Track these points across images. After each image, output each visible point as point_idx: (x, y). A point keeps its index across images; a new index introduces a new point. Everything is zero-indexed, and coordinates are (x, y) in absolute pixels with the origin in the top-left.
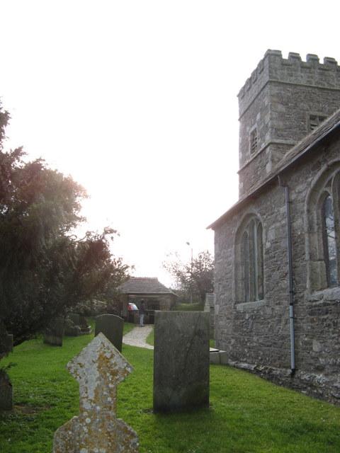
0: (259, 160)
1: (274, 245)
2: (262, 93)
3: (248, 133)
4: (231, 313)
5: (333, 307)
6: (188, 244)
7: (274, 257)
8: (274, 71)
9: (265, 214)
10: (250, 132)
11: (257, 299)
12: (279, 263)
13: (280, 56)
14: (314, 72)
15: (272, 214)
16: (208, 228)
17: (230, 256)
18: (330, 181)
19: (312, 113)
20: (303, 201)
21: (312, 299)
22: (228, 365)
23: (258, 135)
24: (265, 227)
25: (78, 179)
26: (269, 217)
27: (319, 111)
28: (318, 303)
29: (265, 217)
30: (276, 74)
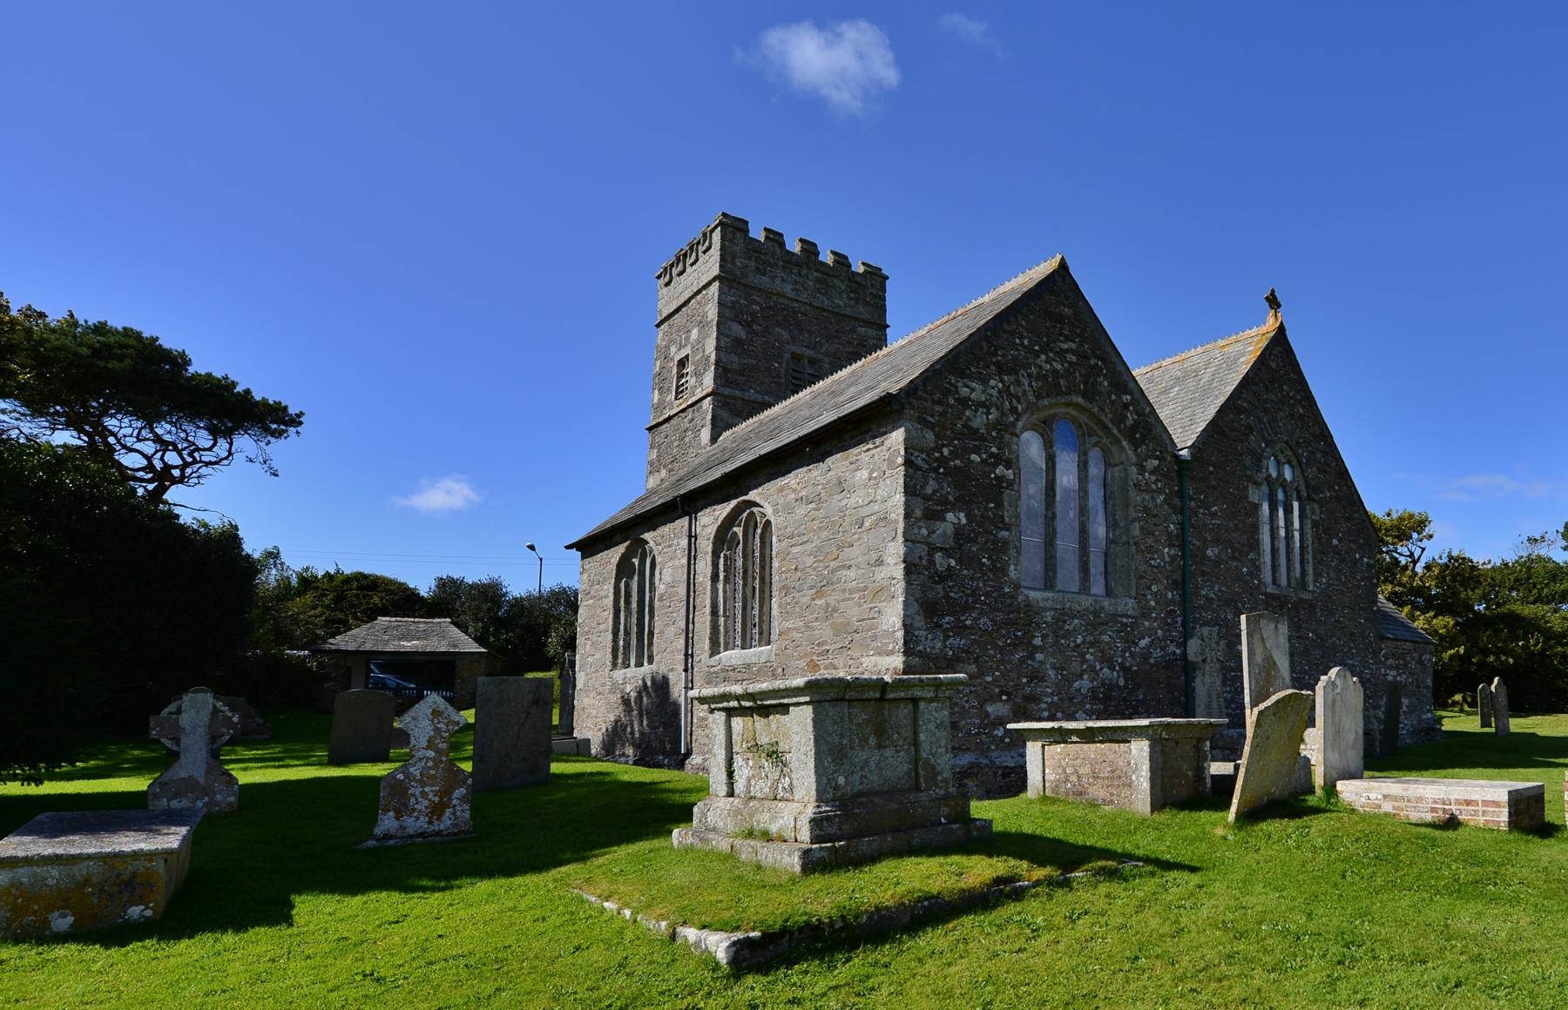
0: (690, 417)
1: (670, 590)
2: (704, 292)
3: (672, 359)
4: (604, 685)
5: (732, 673)
6: (532, 548)
7: (670, 606)
8: (729, 259)
9: (660, 544)
10: (677, 358)
11: (645, 664)
12: (675, 615)
13: (745, 231)
14: (807, 275)
15: (670, 546)
16: (568, 547)
17: (606, 597)
18: (741, 521)
19: (793, 348)
20: (709, 540)
21: (711, 664)
22: (124, 769)
23: (689, 369)
24: (660, 563)
25: (102, 320)
26: (665, 550)
27: (807, 347)
28: (716, 669)
29: (660, 547)
30: (733, 263)
